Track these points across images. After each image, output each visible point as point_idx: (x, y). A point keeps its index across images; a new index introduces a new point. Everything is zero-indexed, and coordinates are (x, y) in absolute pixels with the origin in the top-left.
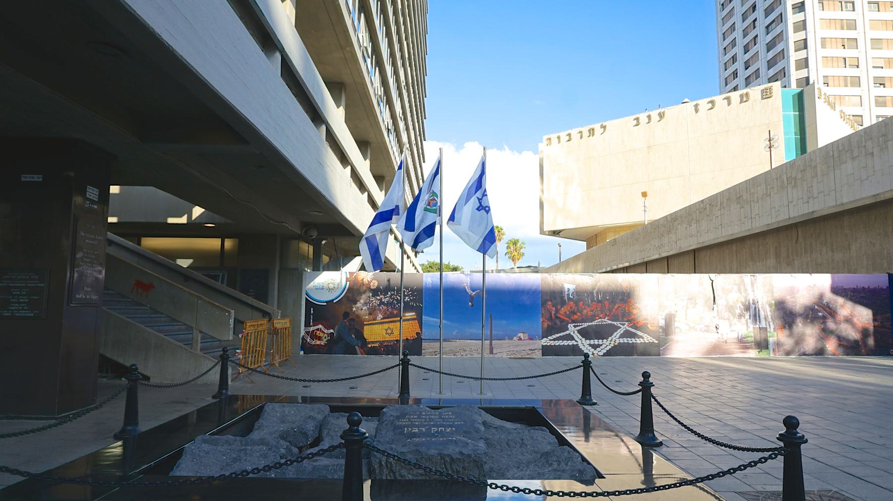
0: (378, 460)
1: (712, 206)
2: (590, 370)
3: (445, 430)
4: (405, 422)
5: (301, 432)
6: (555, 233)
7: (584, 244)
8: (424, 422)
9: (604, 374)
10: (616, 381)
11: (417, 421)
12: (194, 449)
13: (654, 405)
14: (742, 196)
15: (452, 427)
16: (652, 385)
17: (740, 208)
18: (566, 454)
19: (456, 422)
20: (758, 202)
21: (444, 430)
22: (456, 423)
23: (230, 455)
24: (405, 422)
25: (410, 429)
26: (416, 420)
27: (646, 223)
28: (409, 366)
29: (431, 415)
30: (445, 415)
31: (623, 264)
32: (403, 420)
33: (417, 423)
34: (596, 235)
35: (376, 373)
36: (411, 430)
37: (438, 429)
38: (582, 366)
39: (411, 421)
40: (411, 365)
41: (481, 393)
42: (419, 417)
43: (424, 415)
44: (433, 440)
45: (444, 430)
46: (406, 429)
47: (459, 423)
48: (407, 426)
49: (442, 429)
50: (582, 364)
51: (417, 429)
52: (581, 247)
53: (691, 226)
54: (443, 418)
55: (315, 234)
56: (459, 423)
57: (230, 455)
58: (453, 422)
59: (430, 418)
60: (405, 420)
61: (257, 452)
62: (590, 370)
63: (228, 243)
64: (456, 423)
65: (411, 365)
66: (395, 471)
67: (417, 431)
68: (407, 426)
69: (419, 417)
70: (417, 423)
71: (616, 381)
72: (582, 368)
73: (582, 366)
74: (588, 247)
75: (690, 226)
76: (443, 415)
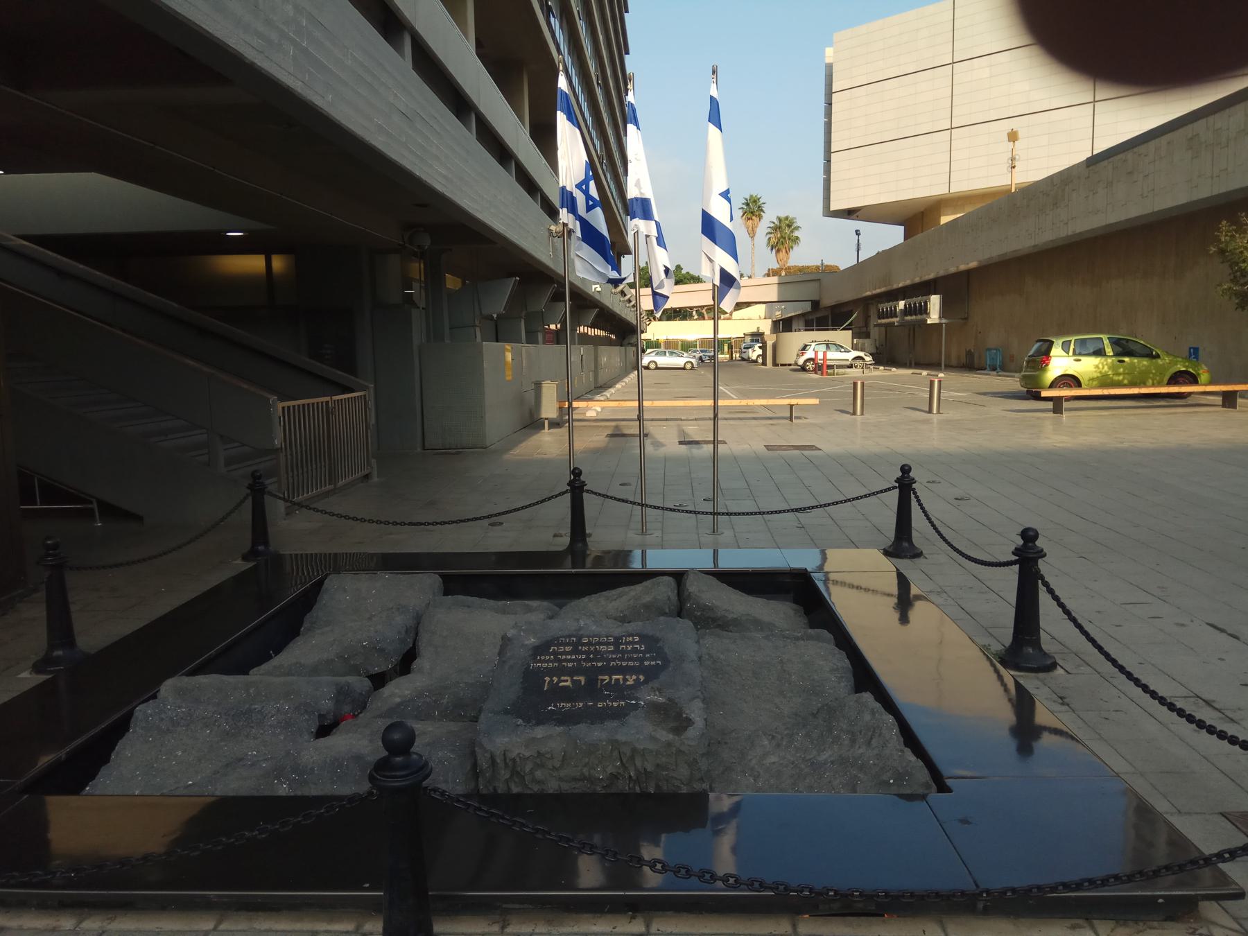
0: (488, 755)
1: (1140, 155)
2: (913, 496)
3: (625, 680)
4: (548, 661)
5: (376, 648)
6: (849, 213)
7: (900, 230)
8: (584, 660)
9: (933, 482)
10: (956, 499)
11: (570, 661)
12: (151, 715)
13: (1044, 597)
14: (1198, 135)
15: (637, 674)
16: (1041, 554)
17: (1192, 158)
18: (867, 717)
19: (647, 659)
20: (1228, 146)
21: (621, 682)
22: (646, 663)
23: (219, 726)
24: (548, 661)
25: (555, 679)
26: (569, 657)
27: (1013, 191)
28: (585, 494)
29: (599, 644)
30: (627, 643)
31: (968, 264)
32: (543, 658)
33: (570, 665)
34: (922, 213)
35: (519, 509)
36: (558, 683)
37: (611, 679)
38: (896, 487)
39: (560, 661)
40: (588, 491)
41: (714, 532)
42: (576, 651)
43: (585, 644)
44: (600, 705)
45: (621, 682)
46: (547, 679)
47: (653, 663)
48: (551, 672)
49: (618, 679)
50: (897, 485)
51: (569, 678)
52: (893, 235)
53: (1097, 193)
54: (623, 652)
55: (426, 242)
56: (653, 663)
57: (219, 726)
58: (642, 660)
59: (596, 652)
60: (547, 658)
61: (272, 716)
62: (913, 496)
63: (278, 263)
64: (646, 663)
65: (588, 491)
66: (523, 774)
67: (568, 683)
68: (551, 672)
69: (576, 651)
70: (570, 665)
71: (956, 499)
72: (897, 490)
73: (896, 487)
74: (907, 236)
75: (1094, 194)
76: (622, 644)
